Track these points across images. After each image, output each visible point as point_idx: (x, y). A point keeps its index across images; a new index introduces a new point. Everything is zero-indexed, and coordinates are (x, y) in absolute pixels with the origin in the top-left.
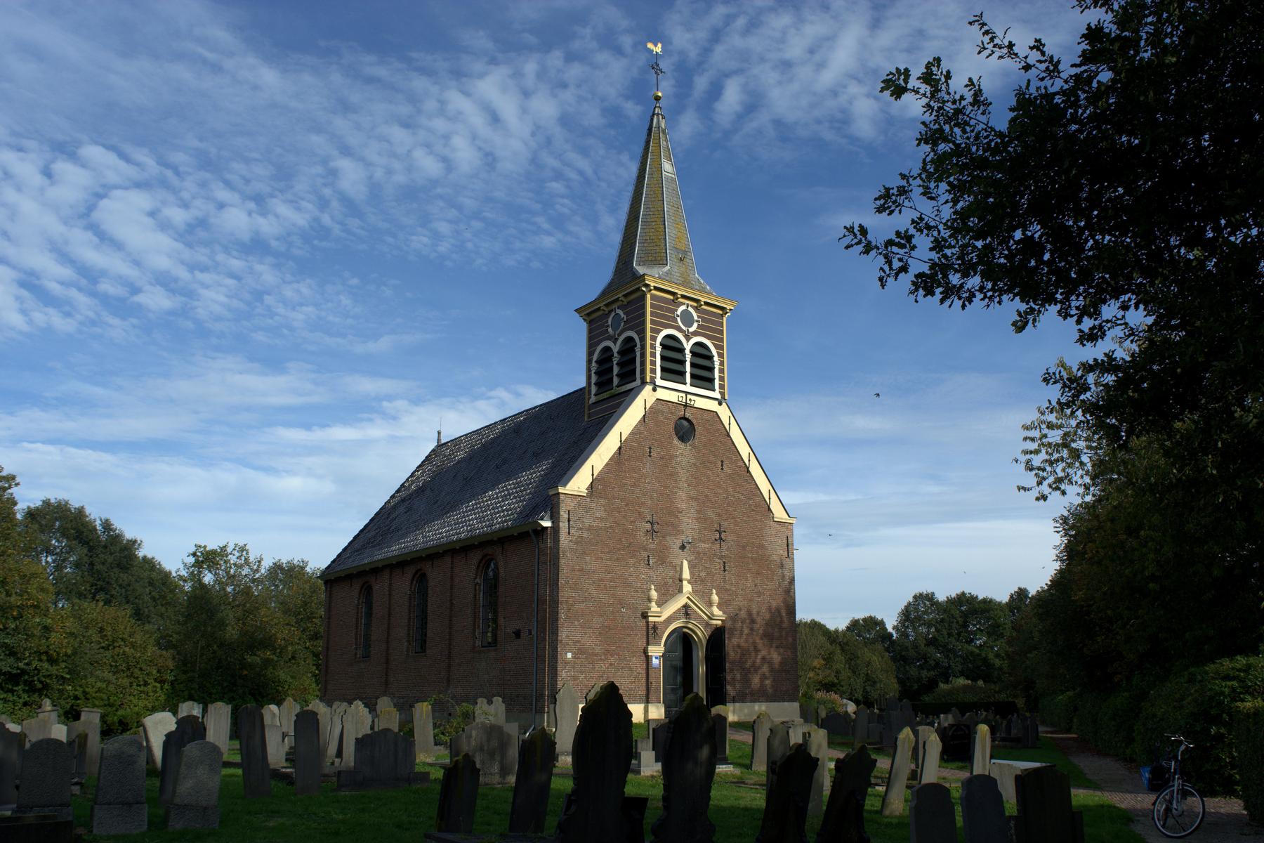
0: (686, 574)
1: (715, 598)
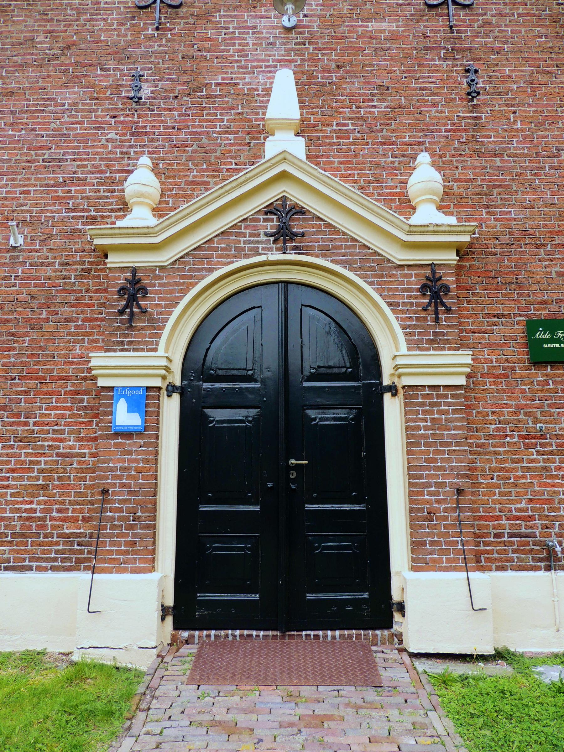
0: (283, 100)
1: (425, 177)
